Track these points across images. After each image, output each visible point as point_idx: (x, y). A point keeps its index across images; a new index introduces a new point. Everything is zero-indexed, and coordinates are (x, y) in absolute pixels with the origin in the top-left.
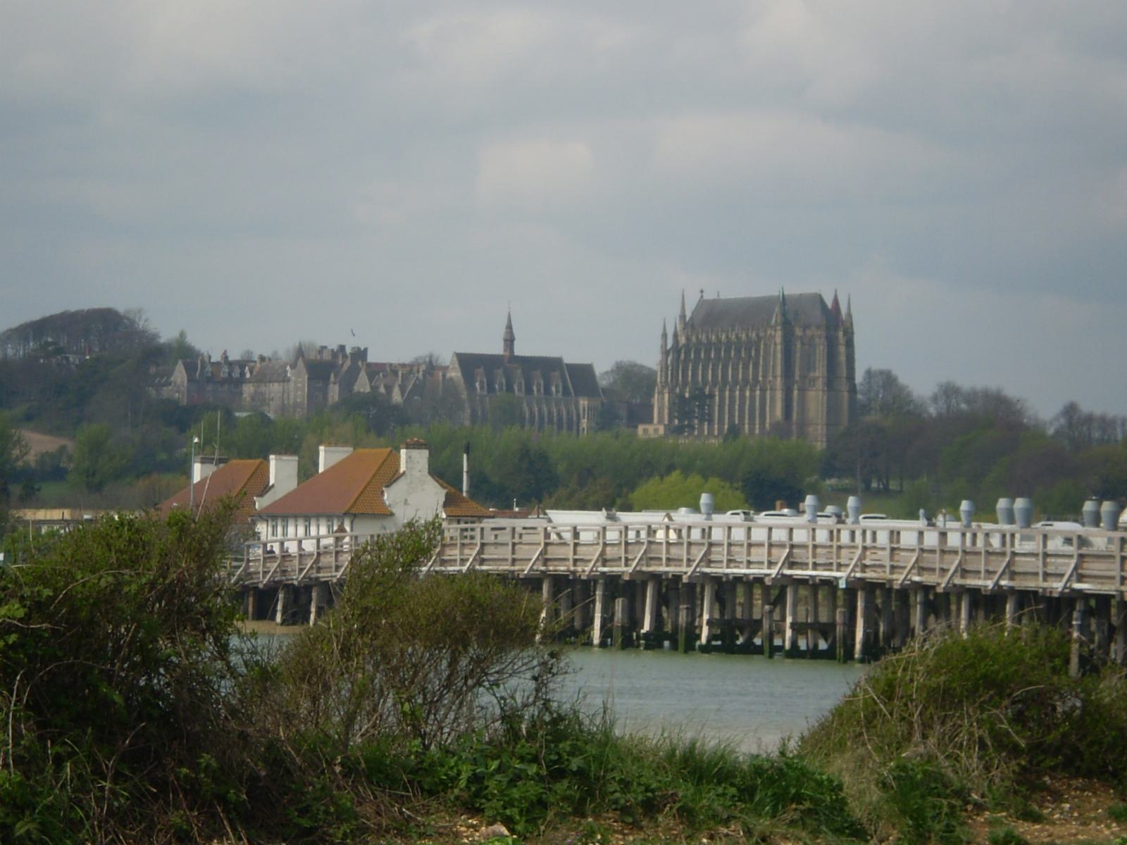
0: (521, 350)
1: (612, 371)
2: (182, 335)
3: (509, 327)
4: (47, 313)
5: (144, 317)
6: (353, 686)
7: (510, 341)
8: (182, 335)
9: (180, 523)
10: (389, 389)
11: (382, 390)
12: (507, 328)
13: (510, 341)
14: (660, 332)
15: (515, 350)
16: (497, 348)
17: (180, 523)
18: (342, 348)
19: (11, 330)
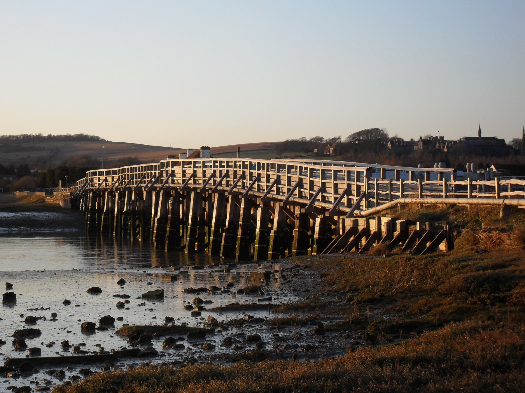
0: (483, 135)
1: (512, 141)
2: (397, 134)
3: (480, 129)
4: (33, 131)
5: (386, 130)
6: (404, 388)
7: (480, 132)
8: (397, 134)
9: (112, 351)
10: (444, 148)
11: (442, 148)
12: (208, 147)
13: (480, 132)
14: (523, 129)
15: (482, 135)
16: (477, 135)
17: (112, 351)
18: (437, 137)
19: (352, 135)
